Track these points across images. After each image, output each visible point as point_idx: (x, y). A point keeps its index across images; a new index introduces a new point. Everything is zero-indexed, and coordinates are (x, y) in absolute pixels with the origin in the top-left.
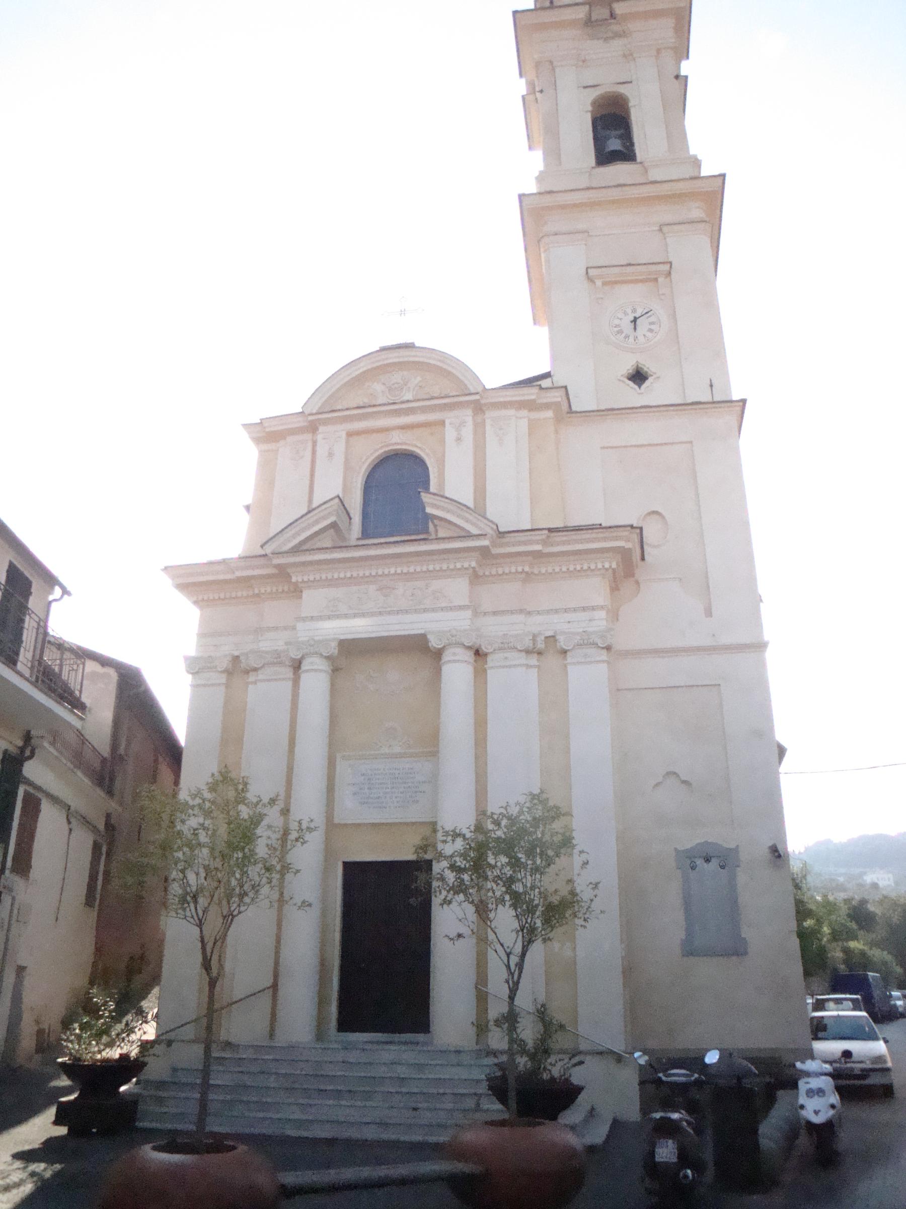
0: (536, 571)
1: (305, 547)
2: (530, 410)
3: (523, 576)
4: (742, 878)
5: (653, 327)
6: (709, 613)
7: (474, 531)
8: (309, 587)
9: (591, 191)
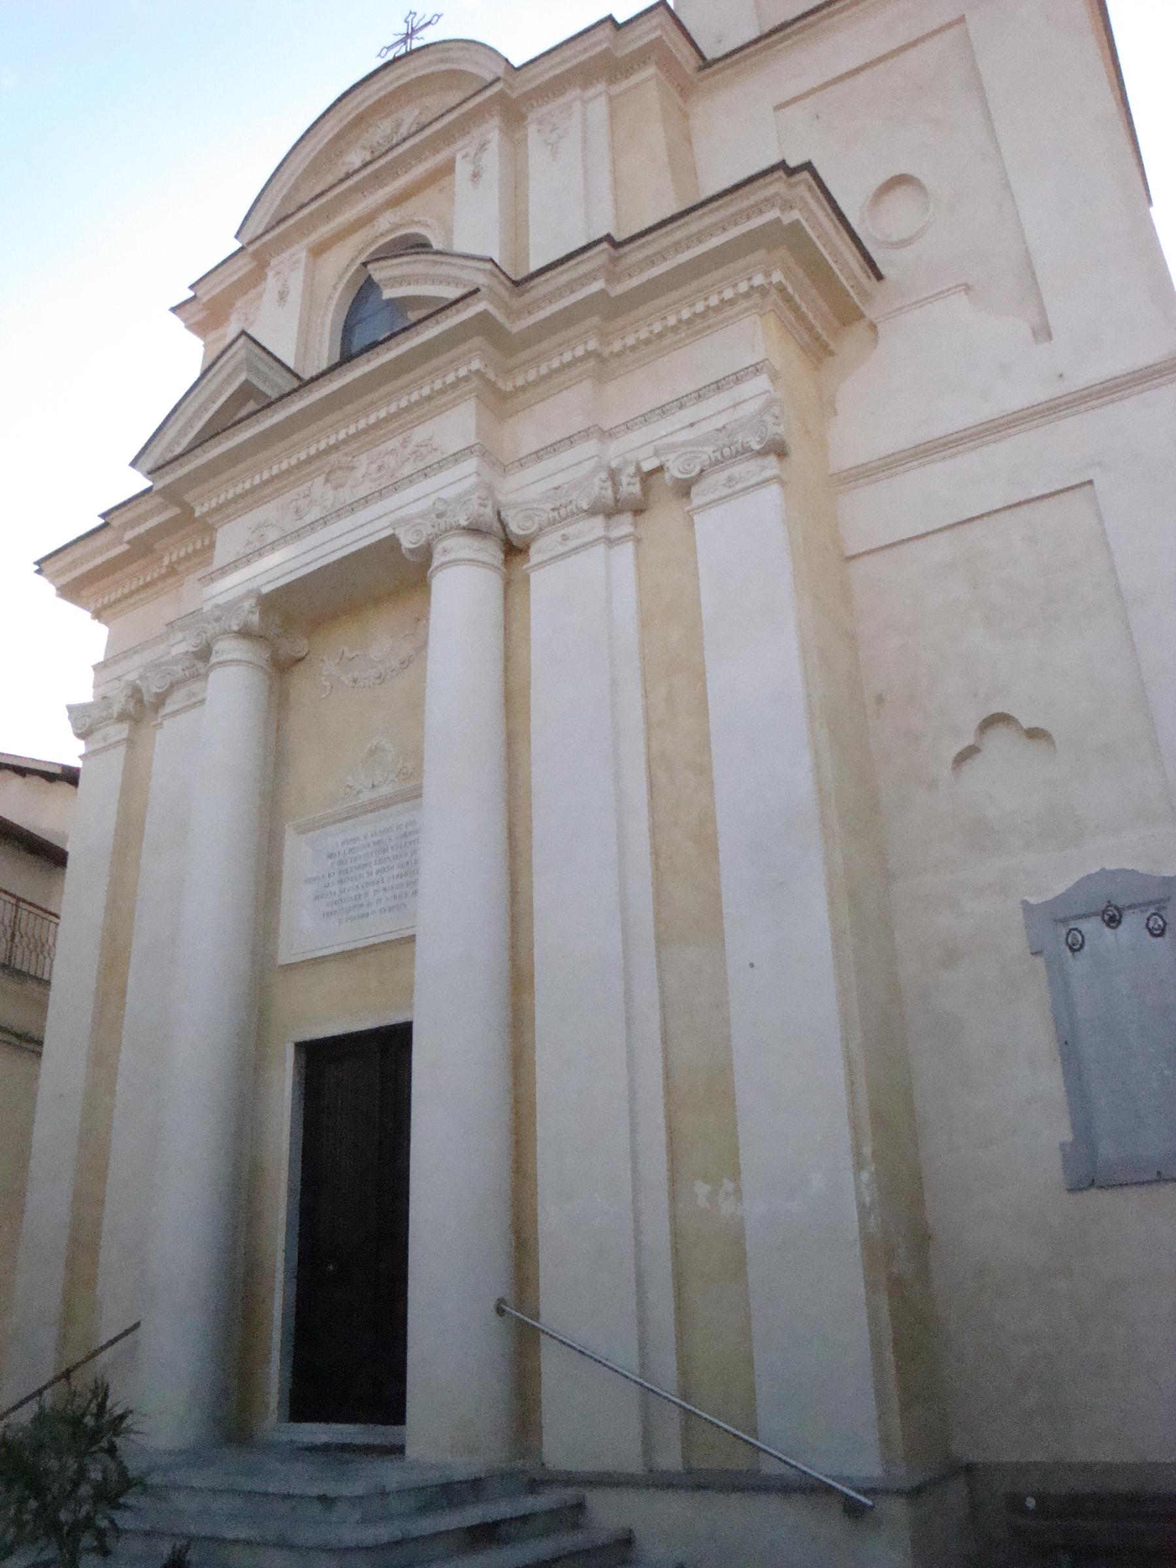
3: (591, 363)
6: (1043, 332)
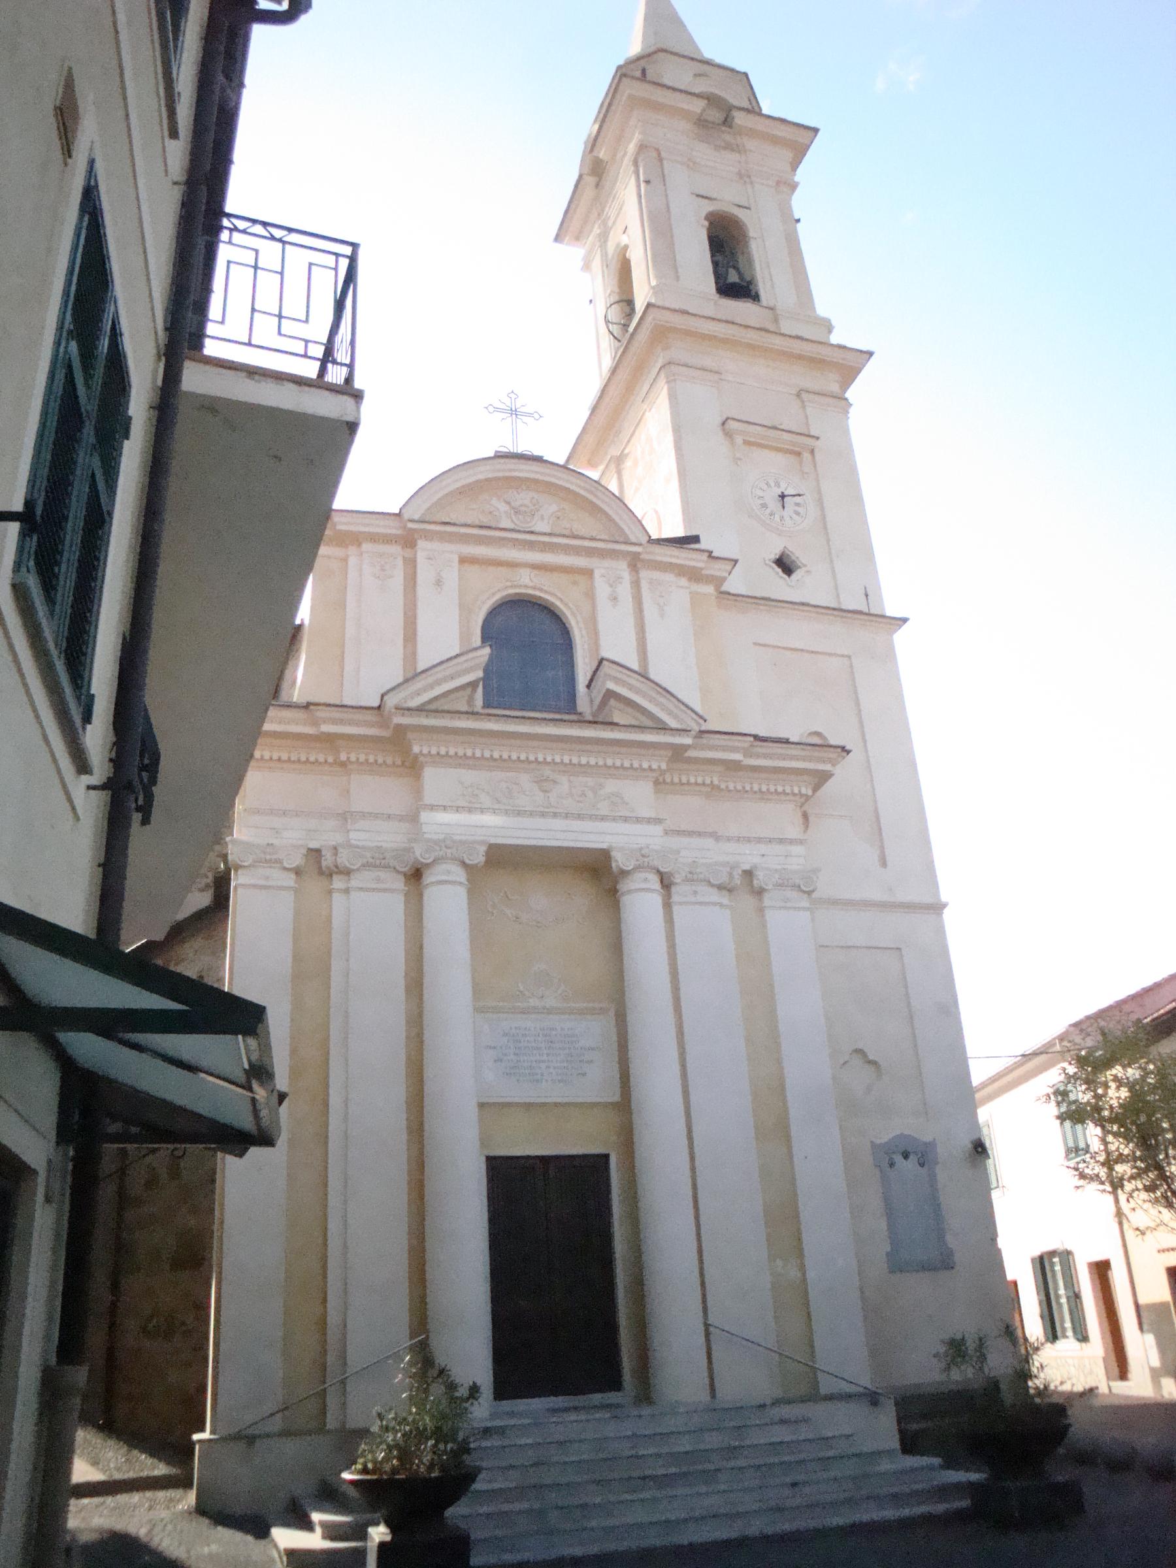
0: (723, 786)
1: (433, 707)
2: (690, 579)
4: (942, 1176)
6: (884, 863)
7: (673, 724)
9: (731, 326)
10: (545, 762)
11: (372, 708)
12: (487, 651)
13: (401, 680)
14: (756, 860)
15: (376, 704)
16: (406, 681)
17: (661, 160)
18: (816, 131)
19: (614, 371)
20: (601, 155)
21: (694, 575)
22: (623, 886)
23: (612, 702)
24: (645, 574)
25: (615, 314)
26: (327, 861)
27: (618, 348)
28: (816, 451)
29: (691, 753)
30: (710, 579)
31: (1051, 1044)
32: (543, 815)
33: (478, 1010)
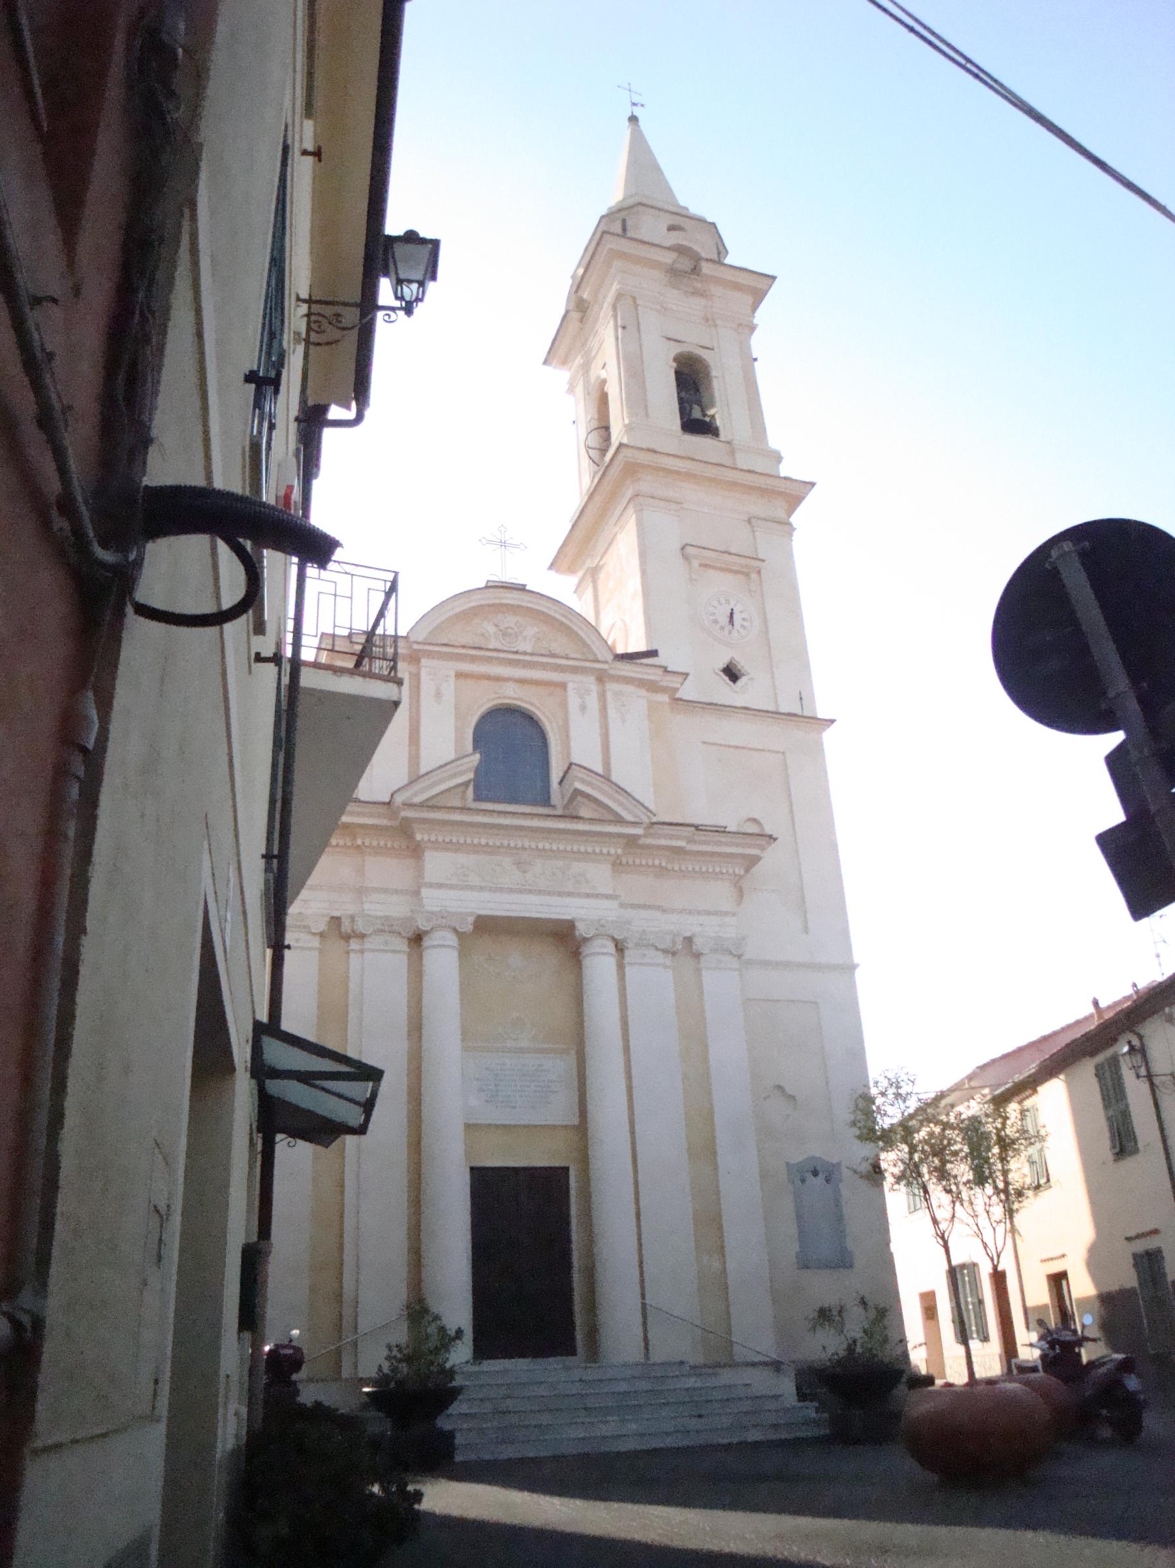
0: (670, 867)
1: (430, 804)
2: (648, 690)
5: (745, 624)
6: (806, 930)
7: (629, 818)
8: (436, 849)
10: (523, 848)
11: (384, 803)
12: (478, 756)
13: (406, 782)
14: (696, 929)
15: (387, 800)
16: (411, 783)
17: (636, 306)
18: (774, 278)
19: (591, 496)
20: (585, 296)
21: (652, 687)
22: (586, 950)
23: (579, 798)
24: (612, 687)
25: (594, 439)
26: (346, 926)
27: (595, 473)
28: (763, 571)
29: (642, 841)
30: (664, 690)
31: (962, 1083)
32: (521, 892)
33: (465, 1049)
